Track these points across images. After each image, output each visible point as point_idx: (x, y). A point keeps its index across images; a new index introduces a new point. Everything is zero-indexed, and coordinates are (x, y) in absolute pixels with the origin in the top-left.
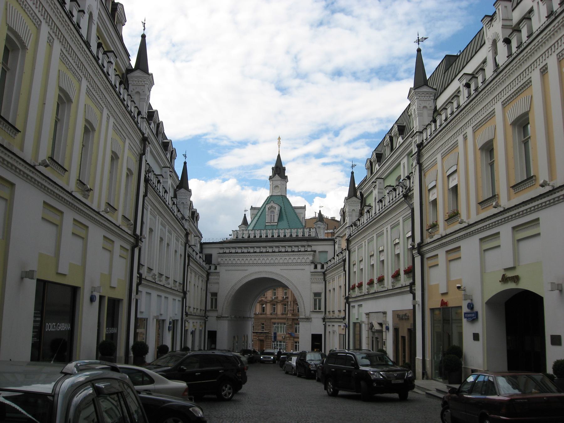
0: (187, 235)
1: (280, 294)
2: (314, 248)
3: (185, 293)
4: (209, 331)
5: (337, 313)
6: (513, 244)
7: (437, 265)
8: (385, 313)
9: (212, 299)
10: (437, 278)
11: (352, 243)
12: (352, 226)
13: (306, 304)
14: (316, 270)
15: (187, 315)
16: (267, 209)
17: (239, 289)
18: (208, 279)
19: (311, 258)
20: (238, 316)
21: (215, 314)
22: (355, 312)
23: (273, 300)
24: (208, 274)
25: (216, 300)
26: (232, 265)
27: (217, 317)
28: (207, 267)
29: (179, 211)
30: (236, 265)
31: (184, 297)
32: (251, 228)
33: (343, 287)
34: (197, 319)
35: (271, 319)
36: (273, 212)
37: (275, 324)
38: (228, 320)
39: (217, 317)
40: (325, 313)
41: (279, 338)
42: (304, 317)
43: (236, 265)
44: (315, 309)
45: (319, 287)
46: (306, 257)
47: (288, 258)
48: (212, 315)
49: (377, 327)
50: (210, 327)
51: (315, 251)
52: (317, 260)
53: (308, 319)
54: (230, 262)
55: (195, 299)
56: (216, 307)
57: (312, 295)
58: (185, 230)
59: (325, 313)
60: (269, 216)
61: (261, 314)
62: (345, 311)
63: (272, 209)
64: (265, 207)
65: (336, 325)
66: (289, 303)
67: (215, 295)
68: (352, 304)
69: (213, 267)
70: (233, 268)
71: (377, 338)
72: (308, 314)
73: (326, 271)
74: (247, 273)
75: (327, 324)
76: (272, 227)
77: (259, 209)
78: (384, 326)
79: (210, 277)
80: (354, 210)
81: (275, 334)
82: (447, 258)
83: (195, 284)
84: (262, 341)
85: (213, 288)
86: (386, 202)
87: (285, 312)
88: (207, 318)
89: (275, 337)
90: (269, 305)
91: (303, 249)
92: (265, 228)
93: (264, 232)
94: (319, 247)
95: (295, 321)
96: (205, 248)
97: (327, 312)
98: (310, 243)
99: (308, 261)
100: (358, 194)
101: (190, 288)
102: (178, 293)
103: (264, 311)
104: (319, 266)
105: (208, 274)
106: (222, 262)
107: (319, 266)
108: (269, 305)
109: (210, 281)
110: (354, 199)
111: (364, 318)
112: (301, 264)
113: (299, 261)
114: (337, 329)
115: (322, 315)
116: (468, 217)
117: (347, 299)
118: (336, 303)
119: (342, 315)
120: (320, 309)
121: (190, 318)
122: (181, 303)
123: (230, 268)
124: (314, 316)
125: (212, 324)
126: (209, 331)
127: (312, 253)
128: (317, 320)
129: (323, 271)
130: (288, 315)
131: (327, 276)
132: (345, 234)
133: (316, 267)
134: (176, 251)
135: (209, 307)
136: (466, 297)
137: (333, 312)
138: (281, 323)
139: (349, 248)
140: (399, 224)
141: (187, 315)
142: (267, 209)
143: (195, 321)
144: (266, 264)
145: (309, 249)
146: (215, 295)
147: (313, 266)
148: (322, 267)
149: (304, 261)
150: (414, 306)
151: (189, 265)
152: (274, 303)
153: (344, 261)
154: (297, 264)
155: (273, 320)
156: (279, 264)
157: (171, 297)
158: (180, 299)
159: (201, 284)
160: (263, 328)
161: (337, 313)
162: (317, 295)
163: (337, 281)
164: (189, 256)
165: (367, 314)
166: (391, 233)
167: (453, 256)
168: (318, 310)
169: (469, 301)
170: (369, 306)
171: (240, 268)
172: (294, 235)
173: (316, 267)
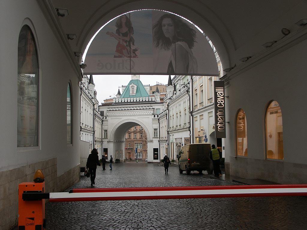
0: (94, 105)
1: (138, 128)
2: (153, 107)
3: (94, 132)
4: (104, 149)
5: (164, 138)
6: (208, 118)
7: (197, 120)
8: (181, 138)
9: (105, 133)
10: (197, 125)
11: (170, 107)
12: (169, 99)
13: (150, 134)
14: (155, 118)
15: (95, 141)
16: (130, 87)
17: (118, 128)
18: (102, 124)
19: (152, 112)
20: (118, 140)
21: (107, 140)
22: (171, 137)
23: (135, 131)
24: (102, 121)
25: (107, 133)
26: (114, 116)
27: (108, 142)
28: (102, 117)
29: (91, 95)
30: (116, 116)
31: (94, 134)
32: (122, 97)
33: (166, 126)
34: (98, 143)
35: (134, 141)
36: (133, 89)
37: (136, 143)
38: (113, 143)
39: (108, 142)
40: (160, 138)
41: (138, 151)
42: (149, 140)
43: (116, 116)
44: (155, 136)
45: (156, 126)
46: (150, 112)
47: (141, 112)
48: (105, 141)
49: (179, 144)
50: (104, 147)
51: (154, 109)
52: (155, 113)
53: (152, 141)
54: (113, 115)
55: (98, 135)
56: (107, 137)
57: (153, 130)
58: (93, 103)
59: (160, 138)
60: (131, 90)
61: (129, 139)
62: (167, 137)
63: (133, 87)
64: (129, 86)
65: (164, 144)
66: (143, 132)
67: (106, 131)
68: (170, 134)
69: (104, 118)
70: (115, 118)
71: (179, 149)
72: (151, 139)
73: (160, 118)
74: (121, 120)
75: (161, 143)
76: (133, 96)
77: (126, 87)
78: (181, 144)
79: (103, 122)
80: (170, 91)
81: (136, 149)
82: (208, 116)
83: (98, 126)
84: (129, 153)
85: (105, 128)
86: (182, 90)
87: (141, 137)
88: (102, 142)
89: (136, 151)
90: (132, 134)
91: (148, 108)
92: (130, 97)
93: (126, 99)
94: (156, 107)
95: (146, 142)
96: (101, 108)
97: (160, 138)
98: (152, 105)
99: (151, 113)
100: (173, 83)
101: (96, 129)
102: (91, 132)
103: (130, 137)
104: (156, 116)
105: (102, 121)
106: (109, 115)
107: (156, 116)
108: (132, 134)
109: (103, 124)
110: (171, 86)
111: (174, 141)
112: (147, 115)
113: (146, 114)
114: (164, 145)
115: (158, 139)
116: (205, 104)
117: (168, 132)
118: (164, 134)
119: (166, 139)
120: (157, 136)
121: (97, 143)
122: (93, 136)
123: (113, 118)
124: (154, 140)
125: (105, 145)
126: (104, 149)
127: (153, 109)
128: (156, 141)
129: (158, 118)
130: (143, 139)
131: (160, 121)
132: (167, 102)
133: (155, 116)
134: (85, 110)
135: (103, 137)
136: (204, 133)
137: (163, 137)
138: (140, 143)
139: (169, 109)
140: (186, 102)
141: (95, 141)
142: (130, 87)
143: (98, 144)
144: (130, 116)
145: (151, 108)
146: (106, 131)
147: (153, 116)
148: (158, 117)
149: (149, 113)
150: (190, 136)
151: (95, 119)
152: (135, 132)
153: (167, 114)
154: (145, 115)
155: (135, 142)
156: (137, 115)
157: (89, 134)
158: (92, 134)
159: (100, 126)
160: (130, 146)
161: (164, 138)
162: (155, 129)
163: (164, 123)
164: (95, 115)
165: (176, 139)
166: (183, 105)
167: (201, 117)
168: (156, 137)
169: (205, 135)
170: (177, 135)
171: (118, 118)
172: (144, 100)
173: (155, 116)
